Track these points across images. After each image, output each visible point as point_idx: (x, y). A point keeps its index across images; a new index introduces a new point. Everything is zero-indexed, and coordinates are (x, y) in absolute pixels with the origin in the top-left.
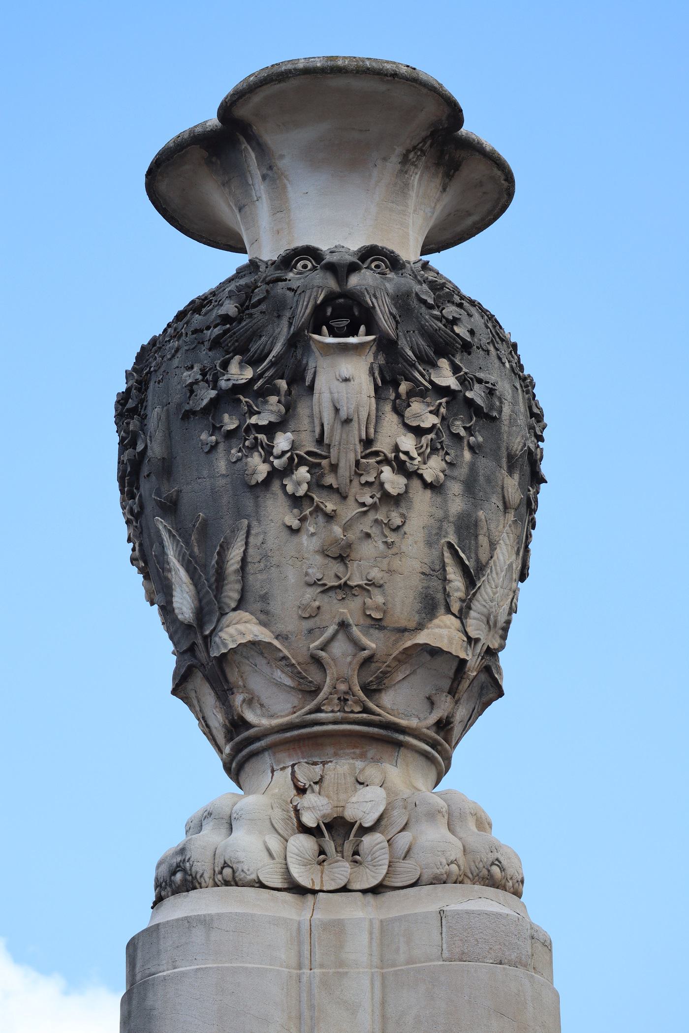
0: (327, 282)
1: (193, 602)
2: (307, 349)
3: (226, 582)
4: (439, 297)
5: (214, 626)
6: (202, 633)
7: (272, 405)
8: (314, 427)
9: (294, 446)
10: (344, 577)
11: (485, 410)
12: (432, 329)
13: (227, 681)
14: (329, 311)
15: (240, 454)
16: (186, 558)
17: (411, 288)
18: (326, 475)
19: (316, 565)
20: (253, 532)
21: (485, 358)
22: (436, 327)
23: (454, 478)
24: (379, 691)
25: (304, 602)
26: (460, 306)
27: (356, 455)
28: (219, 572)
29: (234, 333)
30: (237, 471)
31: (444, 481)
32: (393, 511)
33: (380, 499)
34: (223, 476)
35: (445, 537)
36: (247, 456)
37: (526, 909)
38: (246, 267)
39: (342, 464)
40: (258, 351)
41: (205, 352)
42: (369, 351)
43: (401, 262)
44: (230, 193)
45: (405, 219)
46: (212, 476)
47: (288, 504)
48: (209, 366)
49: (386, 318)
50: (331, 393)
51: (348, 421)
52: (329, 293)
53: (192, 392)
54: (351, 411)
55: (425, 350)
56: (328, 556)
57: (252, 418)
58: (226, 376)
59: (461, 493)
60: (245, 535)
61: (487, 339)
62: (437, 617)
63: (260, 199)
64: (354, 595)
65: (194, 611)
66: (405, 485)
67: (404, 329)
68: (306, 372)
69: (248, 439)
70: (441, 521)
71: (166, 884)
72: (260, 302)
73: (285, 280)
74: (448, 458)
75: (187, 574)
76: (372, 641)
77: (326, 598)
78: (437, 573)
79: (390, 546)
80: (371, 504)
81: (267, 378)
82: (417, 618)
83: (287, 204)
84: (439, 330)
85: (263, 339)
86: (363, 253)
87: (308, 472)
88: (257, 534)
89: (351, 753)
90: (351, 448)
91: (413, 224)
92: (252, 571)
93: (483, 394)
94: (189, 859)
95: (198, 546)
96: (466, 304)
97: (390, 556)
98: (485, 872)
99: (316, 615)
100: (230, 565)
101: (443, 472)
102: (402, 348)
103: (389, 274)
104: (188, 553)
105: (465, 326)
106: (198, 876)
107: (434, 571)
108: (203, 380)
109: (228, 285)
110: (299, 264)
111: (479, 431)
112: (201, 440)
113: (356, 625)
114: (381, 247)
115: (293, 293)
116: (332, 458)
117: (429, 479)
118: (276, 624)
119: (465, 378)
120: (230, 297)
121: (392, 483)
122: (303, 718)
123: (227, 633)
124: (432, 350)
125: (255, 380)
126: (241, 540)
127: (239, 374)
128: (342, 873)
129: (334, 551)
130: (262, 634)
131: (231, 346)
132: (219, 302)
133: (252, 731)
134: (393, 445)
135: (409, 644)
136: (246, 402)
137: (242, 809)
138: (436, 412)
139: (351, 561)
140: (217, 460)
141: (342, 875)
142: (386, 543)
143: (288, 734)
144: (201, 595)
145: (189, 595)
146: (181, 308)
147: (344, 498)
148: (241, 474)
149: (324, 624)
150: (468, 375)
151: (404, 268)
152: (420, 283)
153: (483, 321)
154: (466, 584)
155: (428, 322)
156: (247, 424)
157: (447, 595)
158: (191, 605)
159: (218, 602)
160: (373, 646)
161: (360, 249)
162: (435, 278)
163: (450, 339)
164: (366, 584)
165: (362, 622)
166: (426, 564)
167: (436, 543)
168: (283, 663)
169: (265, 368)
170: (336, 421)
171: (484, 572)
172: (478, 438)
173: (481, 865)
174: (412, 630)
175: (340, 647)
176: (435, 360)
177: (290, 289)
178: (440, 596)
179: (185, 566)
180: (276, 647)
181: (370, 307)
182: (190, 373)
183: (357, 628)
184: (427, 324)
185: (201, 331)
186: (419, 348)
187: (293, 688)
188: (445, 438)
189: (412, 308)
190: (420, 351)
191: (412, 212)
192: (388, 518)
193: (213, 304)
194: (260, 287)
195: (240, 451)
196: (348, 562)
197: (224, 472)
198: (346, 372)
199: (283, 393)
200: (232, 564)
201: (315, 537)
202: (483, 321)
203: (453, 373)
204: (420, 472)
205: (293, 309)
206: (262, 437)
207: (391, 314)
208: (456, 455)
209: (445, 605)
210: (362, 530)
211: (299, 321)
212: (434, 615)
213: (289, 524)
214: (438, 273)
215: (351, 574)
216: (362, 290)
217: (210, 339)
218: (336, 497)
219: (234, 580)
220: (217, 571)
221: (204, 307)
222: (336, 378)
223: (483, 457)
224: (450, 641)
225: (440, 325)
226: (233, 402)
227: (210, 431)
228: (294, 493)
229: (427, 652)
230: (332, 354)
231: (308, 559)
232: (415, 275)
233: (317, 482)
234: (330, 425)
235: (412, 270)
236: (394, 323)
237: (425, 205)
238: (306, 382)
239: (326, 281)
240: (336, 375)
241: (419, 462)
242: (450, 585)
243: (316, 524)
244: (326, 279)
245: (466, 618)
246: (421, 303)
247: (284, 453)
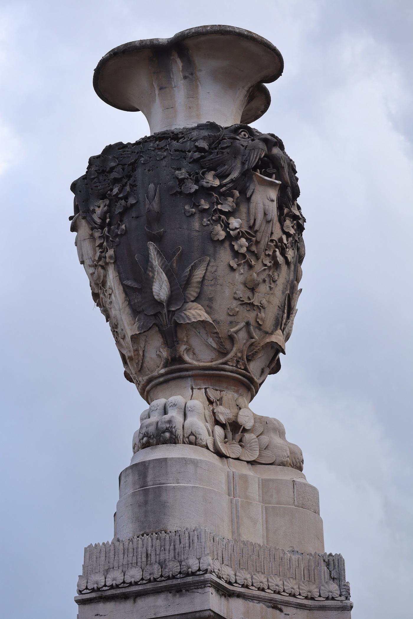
1: (168, 292)
2: (251, 180)
3: (190, 286)
5: (179, 307)
13: (176, 336)
15: (209, 222)
25: (232, 307)
34: (197, 231)
37: (122, 472)
40: (223, 172)
41: (186, 163)
50: (264, 205)
56: (246, 286)
68: (247, 190)
71: (154, 437)
72: (227, 147)
77: (242, 307)
81: (228, 188)
83: (197, 95)
85: (226, 166)
88: (213, 266)
89: (233, 389)
92: (206, 284)
94: (175, 427)
95: (176, 263)
106: (178, 437)
118: (214, 314)
122: (218, 366)
128: (238, 450)
129: (250, 285)
131: (207, 165)
133: (186, 365)
137: (195, 407)
141: (237, 451)
143: (207, 372)
158: (167, 293)
168: (215, 335)
173: (298, 461)
175: (242, 336)
187: (214, 348)
195: (209, 220)
199: (236, 197)
200: (197, 278)
228: (237, 251)
231: (237, 286)
243: (244, 269)
247: (236, 229)
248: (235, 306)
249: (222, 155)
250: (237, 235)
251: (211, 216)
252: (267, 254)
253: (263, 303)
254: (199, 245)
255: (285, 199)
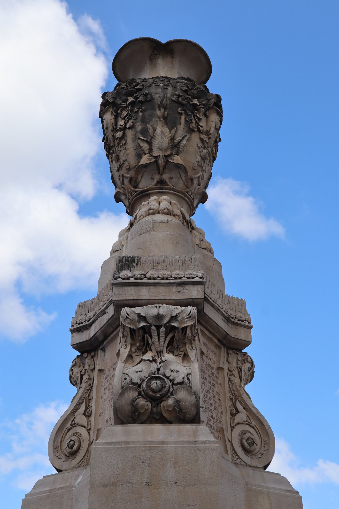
24: (137, 185)
70: (135, 134)
82: (137, 161)
98: (148, 213)
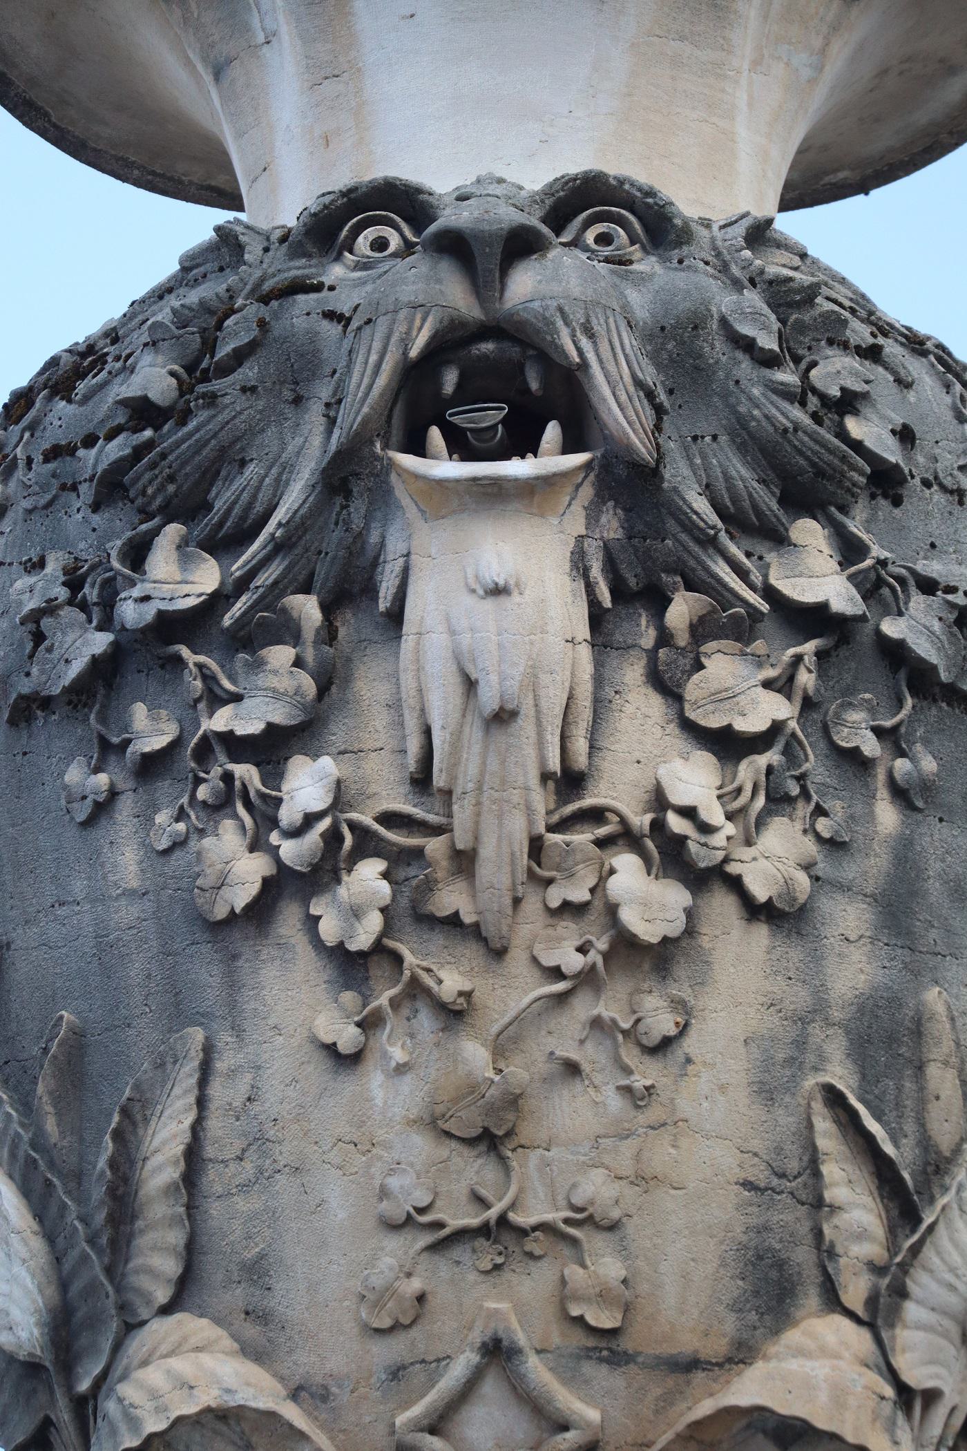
0: (442, 292)
1: (40, 1291)
2: (382, 498)
3: (140, 1224)
4: (801, 328)
6: (69, 1387)
7: (275, 672)
8: (404, 737)
9: (340, 799)
10: (500, 1200)
11: (944, 676)
12: (771, 429)
14: (450, 380)
15: (181, 827)
16: (21, 1154)
17: (706, 303)
18: (440, 886)
19: (412, 1165)
20: (220, 1065)
21: (950, 513)
22: (784, 421)
23: (844, 888)
25: (377, 1281)
26: (872, 354)
27: (531, 822)
28: (120, 1192)
29: (163, 456)
30: (172, 878)
31: (810, 897)
32: (650, 992)
33: (607, 956)
34: (130, 894)
35: (816, 1069)
36: (202, 832)
38: (207, 250)
39: (487, 851)
41: (79, 516)
42: (573, 499)
43: (678, 222)
44: (186, 20)
45: (723, 91)
46: (98, 898)
47: (326, 978)
48: (91, 557)
49: (623, 397)
50: (452, 632)
51: (503, 717)
52: (446, 323)
53: (39, 637)
54: (513, 686)
55: (750, 495)
56: (449, 1135)
57: (216, 716)
58: (139, 586)
59: (868, 934)
60: (197, 1076)
61: (958, 456)
62: (795, 1323)
63: (274, 40)
64: (530, 1255)
65: (46, 1317)
66: (685, 910)
67: (685, 431)
69: (205, 780)
70: (803, 1020)
72: (240, 357)
73: (318, 288)
74: (823, 825)
75: (24, 1201)
76: (590, 1401)
77: (443, 1266)
78: (793, 1184)
79: (642, 1099)
80: (580, 973)
81: (261, 590)
82: (730, 1325)
84: (796, 430)
85: (252, 470)
86: (559, 198)
87: (386, 875)
88: (233, 1073)
90: (516, 799)
91: (750, 105)
92: (218, 1189)
93: (937, 626)
96: (891, 348)
97: (641, 1130)
99: (413, 1322)
100: (154, 1171)
101: (807, 867)
102: (675, 489)
103: (639, 261)
104: (26, 1136)
105: (883, 417)
107: (782, 1176)
108: (70, 602)
109: (154, 307)
110: (361, 239)
111: (926, 742)
112: (66, 787)
113: (539, 1352)
114: (615, 178)
115: (340, 328)
116: (458, 833)
117: (760, 892)
118: (290, 1352)
119: (879, 576)
120: (154, 344)
121: (645, 904)
123: (141, 1386)
124: (773, 494)
125: (227, 597)
126: (186, 1092)
127: (179, 579)
129: (469, 1120)
130: (248, 1384)
131: (154, 497)
132: (126, 361)
134: (650, 787)
135: (705, 1408)
136: (200, 666)
138: (783, 685)
139: (520, 1150)
140: (115, 846)
142: (627, 1090)
144: (65, 1272)
145: (28, 1269)
146: (22, 381)
147: (499, 953)
148: (184, 886)
149: (439, 1349)
150: (891, 568)
151: (688, 243)
152: (737, 285)
153: (948, 400)
154: (888, 1218)
155: (757, 407)
156: (200, 732)
157: (826, 1252)
158: (34, 1301)
159: (119, 1289)
160: (594, 1415)
161: (550, 185)
162: (796, 269)
163: (827, 457)
164: (567, 1221)
165: (556, 1340)
166: (756, 1154)
167: (788, 1089)
169: (254, 562)
170: (469, 718)
171: (947, 1180)
172: (923, 763)
174: (717, 1364)
176: (783, 524)
177: (330, 315)
178: (803, 1256)
179: (17, 1176)
180: (291, 1426)
181: (571, 363)
182: (31, 580)
183: (541, 1360)
184: (756, 412)
185: (70, 450)
186: (731, 488)
188: (813, 763)
189: (710, 365)
190: (735, 499)
191: (746, 66)
192: (635, 1012)
193: (108, 367)
194: (240, 310)
195: (181, 815)
196: (509, 1154)
197: (134, 884)
198: (495, 567)
199: (309, 634)
200: (159, 1168)
201: (408, 1078)
202: (948, 400)
203: (840, 564)
204: (732, 868)
205: (337, 375)
206: (246, 772)
207: (639, 384)
208: (852, 817)
209: (823, 1285)
210: (552, 1053)
211: (352, 416)
212: (788, 1315)
213: (328, 1039)
214: (803, 256)
215: (521, 1190)
216: (547, 314)
217: (94, 476)
218: (471, 952)
219: (164, 1217)
220: (112, 1191)
221: (83, 376)
222: (467, 585)
223: (941, 820)
224: (839, 1396)
225: (797, 413)
226: (162, 667)
227: (92, 757)
228: (341, 944)
229: (765, 1432)
230: (454, 512)
231: (387, 1146)
232: (724, 261)
233: (414, 908)
234: (450, 730)
235: (715, 248)
236: (650, 412)
237: (790, 43)
238: (381, 601)
239: (437, 287)
240: (466, 578)
241: (729, 838)
242: (836, 1220)
243: (412, 1036)
244: (439, 281)
245: (892, 1326)
246: (738, 348)
247: (310, 819)
248: (391, 1269)
249: (212, 412)
250: (319, 855)
251: (190, 786)
252: (555, 904)
253: (592, 1202)
254: (149, 976)
255: (669, 542)
